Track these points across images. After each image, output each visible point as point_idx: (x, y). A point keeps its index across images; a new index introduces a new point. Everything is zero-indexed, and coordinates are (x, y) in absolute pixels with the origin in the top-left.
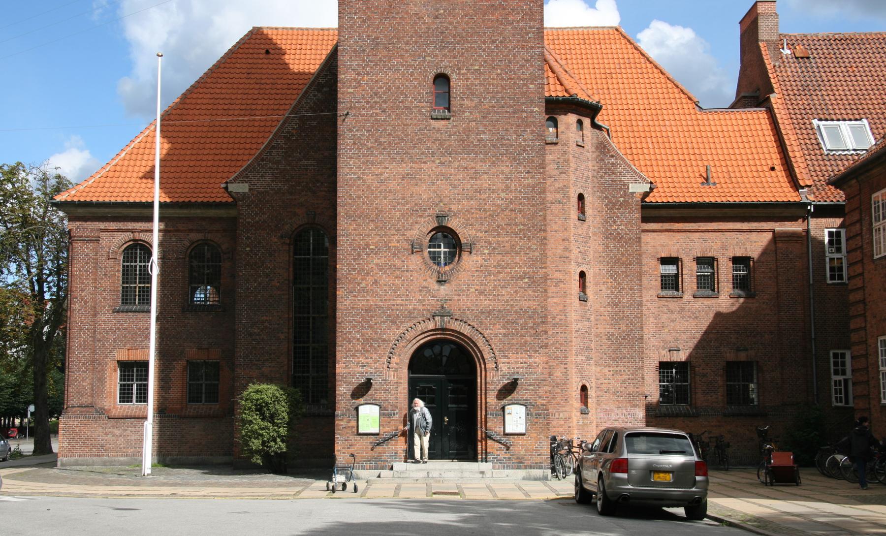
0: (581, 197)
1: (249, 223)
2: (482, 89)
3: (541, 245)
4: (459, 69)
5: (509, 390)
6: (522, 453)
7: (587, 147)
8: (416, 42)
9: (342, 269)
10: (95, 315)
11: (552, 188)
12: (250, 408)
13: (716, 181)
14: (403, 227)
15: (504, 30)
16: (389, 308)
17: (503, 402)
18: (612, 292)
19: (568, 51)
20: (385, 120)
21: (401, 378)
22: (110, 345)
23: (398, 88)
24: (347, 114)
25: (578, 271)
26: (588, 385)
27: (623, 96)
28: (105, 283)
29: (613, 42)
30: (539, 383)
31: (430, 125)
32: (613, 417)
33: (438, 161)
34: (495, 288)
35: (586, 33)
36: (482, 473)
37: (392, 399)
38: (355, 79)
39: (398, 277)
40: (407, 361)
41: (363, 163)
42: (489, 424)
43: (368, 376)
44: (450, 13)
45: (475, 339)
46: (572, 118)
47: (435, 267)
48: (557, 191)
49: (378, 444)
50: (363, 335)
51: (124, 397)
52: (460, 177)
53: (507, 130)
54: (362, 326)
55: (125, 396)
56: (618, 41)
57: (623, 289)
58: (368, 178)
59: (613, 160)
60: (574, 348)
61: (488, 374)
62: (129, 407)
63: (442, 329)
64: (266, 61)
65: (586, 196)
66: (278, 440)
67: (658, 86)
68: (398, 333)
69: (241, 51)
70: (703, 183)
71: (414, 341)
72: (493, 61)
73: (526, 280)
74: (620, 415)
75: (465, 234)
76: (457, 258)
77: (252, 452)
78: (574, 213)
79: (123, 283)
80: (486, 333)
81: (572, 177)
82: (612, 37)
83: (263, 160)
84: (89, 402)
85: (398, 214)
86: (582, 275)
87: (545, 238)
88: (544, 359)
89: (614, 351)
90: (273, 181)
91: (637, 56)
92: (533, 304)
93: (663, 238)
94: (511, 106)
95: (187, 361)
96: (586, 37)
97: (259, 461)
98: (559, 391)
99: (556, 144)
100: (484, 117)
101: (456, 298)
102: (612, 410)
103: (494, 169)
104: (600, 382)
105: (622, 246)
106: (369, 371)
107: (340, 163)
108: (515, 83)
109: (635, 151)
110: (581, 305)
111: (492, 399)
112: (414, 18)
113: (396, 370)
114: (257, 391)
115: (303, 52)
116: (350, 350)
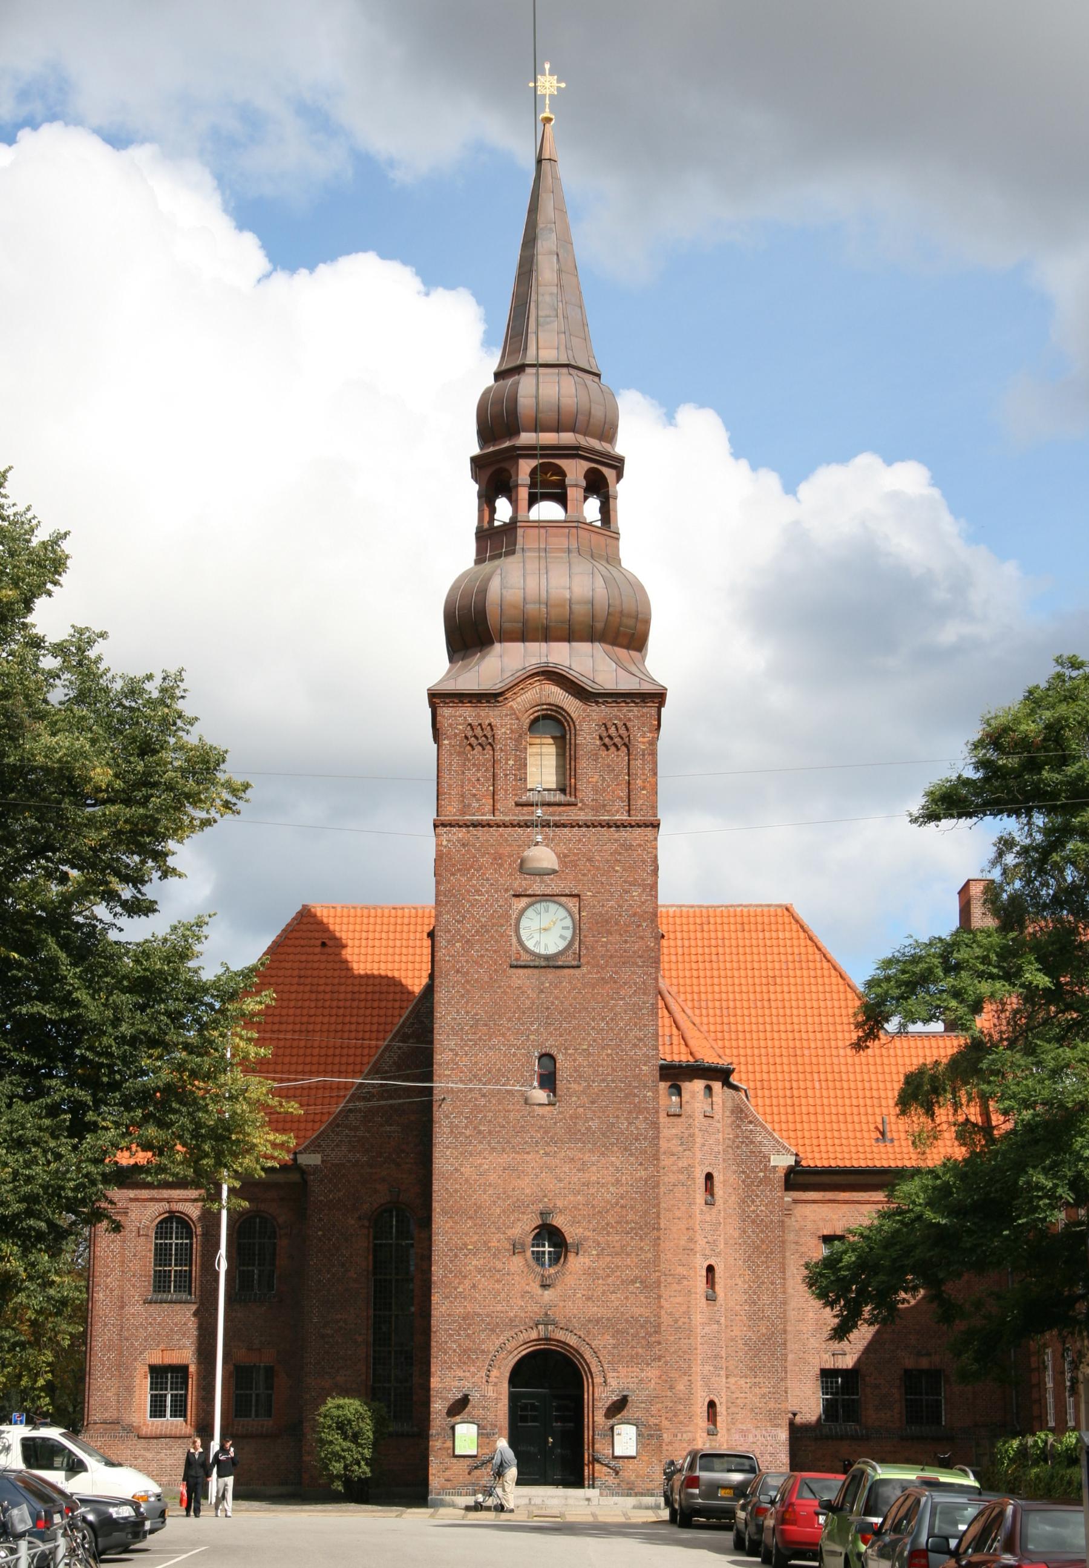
0: (709, 1177)
1: (321, 1201)
2: (590, 1071)
3: (654, 1246)
4: (566, 1049)
5: (618, 1407)
6: (633, 1478)
7: (717, 1117)
8: (519, 1019)
9: (437, 1271)
10: (122, 1307)
11: (675, 1168)
12: (330, 1427)
13: (895, 1135)
14: (504, 1225)
15: (615, 1005)
16: (488, 1316)
17: (611, 1422)
18: (750, 1286)
19: (720, 942)
20: (485, 1106)
21: (501, 1394)
22: (140, 1345)
23: (499, 1070)
24: (444, 1099)
25: (705, 1265)
26: (716, 1401)
27: (788, 1012)
28: (135, 1266)
29: (780, 927)
30: (651, 1400)
31: (534, 1111)
32: (751, 1439)
33: (542, 1152)
34: (604, 1293)
35: (745, 914)
36: (588, 1500)
37: (491, 1417)
38: (453, 1060)
39: (498, 1281)
40: (508, 1375)
41: (461, 1153)
42: (597, 1446)
43: (465, 1391)
44: (556, 987)
45: (582, 1350)
46: (699, 1085)
47: (538, 1269)
48: (681, 1171)
49: (476, 1468)
50: (460, 1346)
51: (155, 1411)
52: (567, 1170)
53: (617, 1117)
54: (459, 1335)
55: (157, 1410)
56: (787, 927)
57: (763, 1283)
58: (467, 1170)
59: (751, 1127)
60: (700, 1357)
61: (596, 1390)
62: (162, 1424)
63: (546, 1339)
64: (324, 958)
65: (715, 1175)
66: (363, 1463)
67: (835, 996)
68: (498, 1343)
69: (290, 942)
70: (877, 1140)
71: (516, 1352)
72: (603, 1039)
73: (638, 1285)
74: (759, 1437)
75: (571, 1233)
76: (562, 1260)
77: (332, 1478)
78: (700, 1196)
79: (155, 1265)
80: (594, 1344)
81: (699, 1155)
82: (780, 920)
83: (338, 1126)
84: (115, 1417)
85: (498, 1211)
86: (710, 1269)
87: (659, 1238)
88: (657, 1373)
89: (751, 1359)
90: (349, 1151)
91: (810, 950)
92: (646, 1312)
93: (824, 1210)
94: (622, 1090)
95: (234, 1365)
96: (746, 920)
97: (340, 1488)
98: (682, 1407)
99: (679, 1116)
100: (593, 1103)
101: (561, 1304)
102: (748, 1430)
103: (603, 1161)
104: (734, 1396)
105: (762, 1231)
106: (466, 1386)
107: (436, 1154)
108: (626, 1065)
109: (796, 1093)
110: (708, 1305)
111: (600, 1418)
112: (517, 992)
113: (496, 1384)
114: (339, 1407)
115: (370, 943)
116: (445, 1362)
